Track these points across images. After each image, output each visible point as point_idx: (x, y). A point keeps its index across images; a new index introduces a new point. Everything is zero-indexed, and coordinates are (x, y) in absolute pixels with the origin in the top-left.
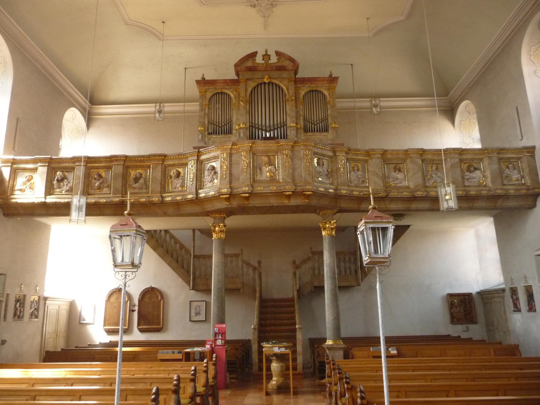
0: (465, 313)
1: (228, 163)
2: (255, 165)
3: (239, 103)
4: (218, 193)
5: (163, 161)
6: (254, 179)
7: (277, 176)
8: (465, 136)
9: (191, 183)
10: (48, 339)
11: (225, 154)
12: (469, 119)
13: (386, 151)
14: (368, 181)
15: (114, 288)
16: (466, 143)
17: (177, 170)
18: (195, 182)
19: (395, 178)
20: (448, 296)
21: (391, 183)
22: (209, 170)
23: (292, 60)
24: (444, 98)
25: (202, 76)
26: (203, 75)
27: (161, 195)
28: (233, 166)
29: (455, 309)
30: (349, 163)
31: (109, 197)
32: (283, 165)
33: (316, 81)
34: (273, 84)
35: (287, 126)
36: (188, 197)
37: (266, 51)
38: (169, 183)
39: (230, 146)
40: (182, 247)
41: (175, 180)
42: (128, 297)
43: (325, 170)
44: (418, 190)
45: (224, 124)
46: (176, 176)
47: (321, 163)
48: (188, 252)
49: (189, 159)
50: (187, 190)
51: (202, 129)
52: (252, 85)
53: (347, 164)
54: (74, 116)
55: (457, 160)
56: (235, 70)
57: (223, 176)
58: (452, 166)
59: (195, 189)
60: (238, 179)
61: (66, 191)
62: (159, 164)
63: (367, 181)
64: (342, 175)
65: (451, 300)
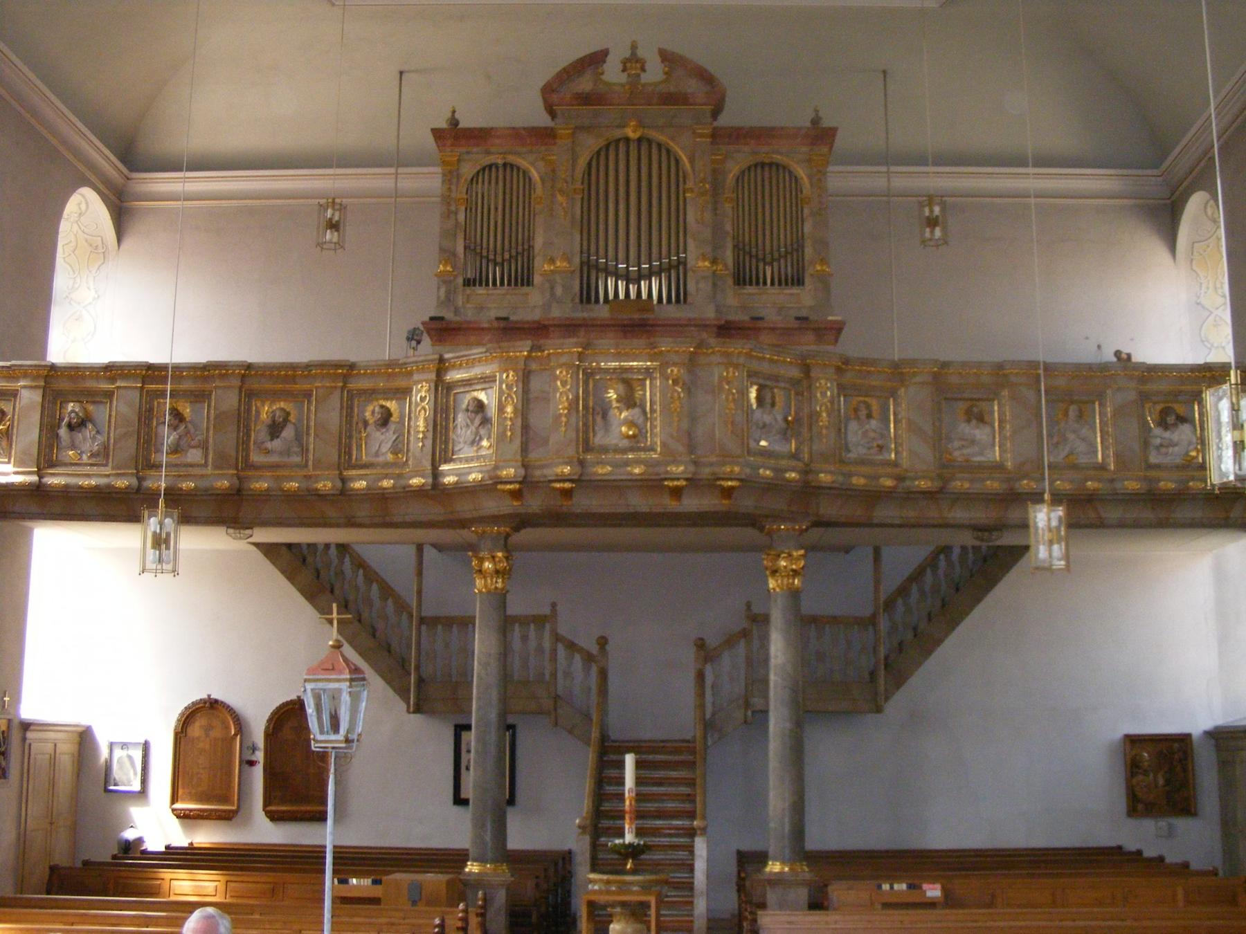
0: (1167, 788)
1: (520, 398)
2: (591, 404)
3: (553, 196)
4: (491, 478)
5: (346, 378)
6: (586, 441)
7: (649, 435)
8: (1204, 286)
9: (420, 444)
10: (32, 831)
11: (511, 373)
12: (1214, 237)
13: (945, 365)
14: (895, 447)
15: (198, 698)
16: (1203, 307)
17: (382, 407)
18: (429, 442)
19: (966, 440)
20: (1124, 743)
21: (957, 453)
22: (467, 410)
23: (706, 77)
24: (1149, 172)
25: (449, 115)
26: (454, 112)
27: (341, 474)
28: (531, 406)
29: (1140, 777)
30: (845, 396)
31: (202, 476)
32: (665, 409)
34: (650, 142)
35: (689, 266)
36: (411, 482)
37: (634, 47)
38: (361, 439)
39: (526, 353)
40: (387, 591)
41: (378, 434)
42: (235, 725)
43: (779, 418)
44: (1025, 476)
45: (511, 257)
46: (379, 422)
47: (768, 400)
48: (402, 607)
49: (416, 377)
50: (410, 462)
51: (449, 268)
52: (590, 144)
53: (839, 401)
54: (83, 207)
55: (1132, 396)
56: (545, 101)
57: (504, 433)
58: (1118, 412)
59: (430, 462)
60: (546, 441)
61: (92, 455)
62: (336, 387)
63: (893, 446)
64: (824, 431)
65: (1134, 752)
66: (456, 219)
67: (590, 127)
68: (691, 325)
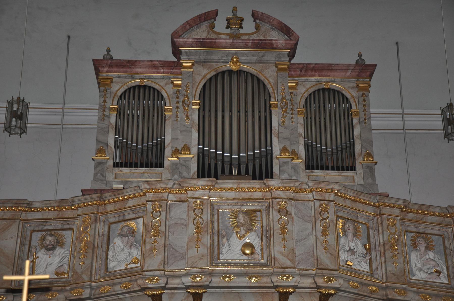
33: (331, 70)
66: (109, 122)
67: (205, 62)
68: (212, 215)
